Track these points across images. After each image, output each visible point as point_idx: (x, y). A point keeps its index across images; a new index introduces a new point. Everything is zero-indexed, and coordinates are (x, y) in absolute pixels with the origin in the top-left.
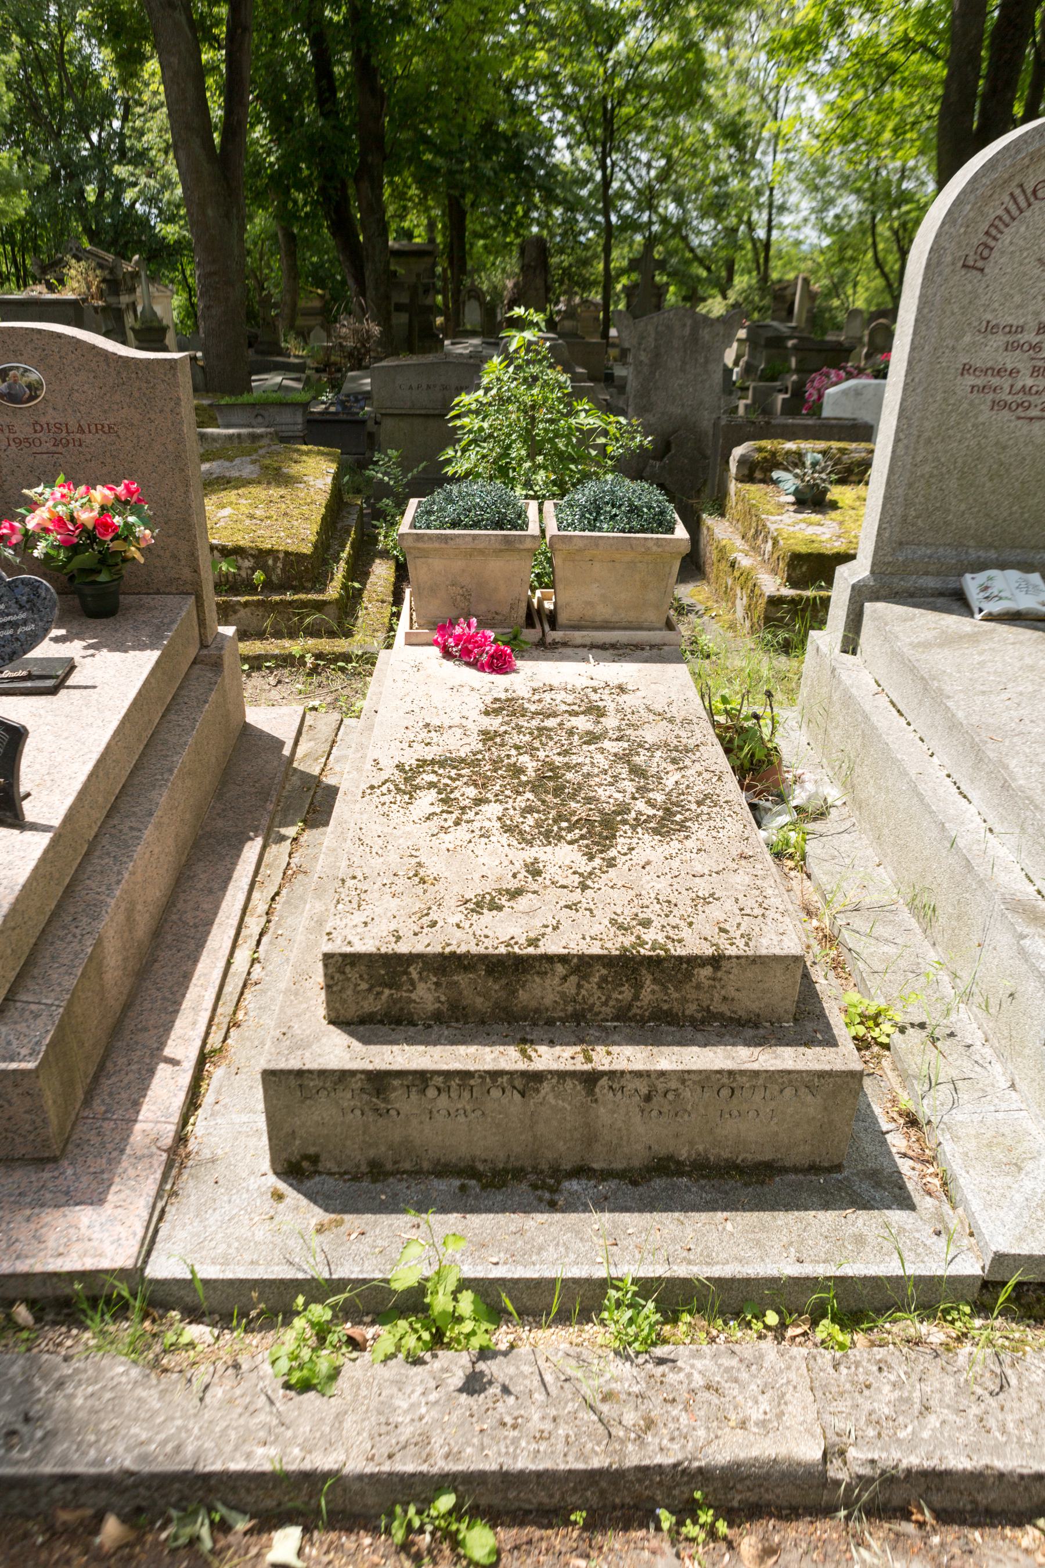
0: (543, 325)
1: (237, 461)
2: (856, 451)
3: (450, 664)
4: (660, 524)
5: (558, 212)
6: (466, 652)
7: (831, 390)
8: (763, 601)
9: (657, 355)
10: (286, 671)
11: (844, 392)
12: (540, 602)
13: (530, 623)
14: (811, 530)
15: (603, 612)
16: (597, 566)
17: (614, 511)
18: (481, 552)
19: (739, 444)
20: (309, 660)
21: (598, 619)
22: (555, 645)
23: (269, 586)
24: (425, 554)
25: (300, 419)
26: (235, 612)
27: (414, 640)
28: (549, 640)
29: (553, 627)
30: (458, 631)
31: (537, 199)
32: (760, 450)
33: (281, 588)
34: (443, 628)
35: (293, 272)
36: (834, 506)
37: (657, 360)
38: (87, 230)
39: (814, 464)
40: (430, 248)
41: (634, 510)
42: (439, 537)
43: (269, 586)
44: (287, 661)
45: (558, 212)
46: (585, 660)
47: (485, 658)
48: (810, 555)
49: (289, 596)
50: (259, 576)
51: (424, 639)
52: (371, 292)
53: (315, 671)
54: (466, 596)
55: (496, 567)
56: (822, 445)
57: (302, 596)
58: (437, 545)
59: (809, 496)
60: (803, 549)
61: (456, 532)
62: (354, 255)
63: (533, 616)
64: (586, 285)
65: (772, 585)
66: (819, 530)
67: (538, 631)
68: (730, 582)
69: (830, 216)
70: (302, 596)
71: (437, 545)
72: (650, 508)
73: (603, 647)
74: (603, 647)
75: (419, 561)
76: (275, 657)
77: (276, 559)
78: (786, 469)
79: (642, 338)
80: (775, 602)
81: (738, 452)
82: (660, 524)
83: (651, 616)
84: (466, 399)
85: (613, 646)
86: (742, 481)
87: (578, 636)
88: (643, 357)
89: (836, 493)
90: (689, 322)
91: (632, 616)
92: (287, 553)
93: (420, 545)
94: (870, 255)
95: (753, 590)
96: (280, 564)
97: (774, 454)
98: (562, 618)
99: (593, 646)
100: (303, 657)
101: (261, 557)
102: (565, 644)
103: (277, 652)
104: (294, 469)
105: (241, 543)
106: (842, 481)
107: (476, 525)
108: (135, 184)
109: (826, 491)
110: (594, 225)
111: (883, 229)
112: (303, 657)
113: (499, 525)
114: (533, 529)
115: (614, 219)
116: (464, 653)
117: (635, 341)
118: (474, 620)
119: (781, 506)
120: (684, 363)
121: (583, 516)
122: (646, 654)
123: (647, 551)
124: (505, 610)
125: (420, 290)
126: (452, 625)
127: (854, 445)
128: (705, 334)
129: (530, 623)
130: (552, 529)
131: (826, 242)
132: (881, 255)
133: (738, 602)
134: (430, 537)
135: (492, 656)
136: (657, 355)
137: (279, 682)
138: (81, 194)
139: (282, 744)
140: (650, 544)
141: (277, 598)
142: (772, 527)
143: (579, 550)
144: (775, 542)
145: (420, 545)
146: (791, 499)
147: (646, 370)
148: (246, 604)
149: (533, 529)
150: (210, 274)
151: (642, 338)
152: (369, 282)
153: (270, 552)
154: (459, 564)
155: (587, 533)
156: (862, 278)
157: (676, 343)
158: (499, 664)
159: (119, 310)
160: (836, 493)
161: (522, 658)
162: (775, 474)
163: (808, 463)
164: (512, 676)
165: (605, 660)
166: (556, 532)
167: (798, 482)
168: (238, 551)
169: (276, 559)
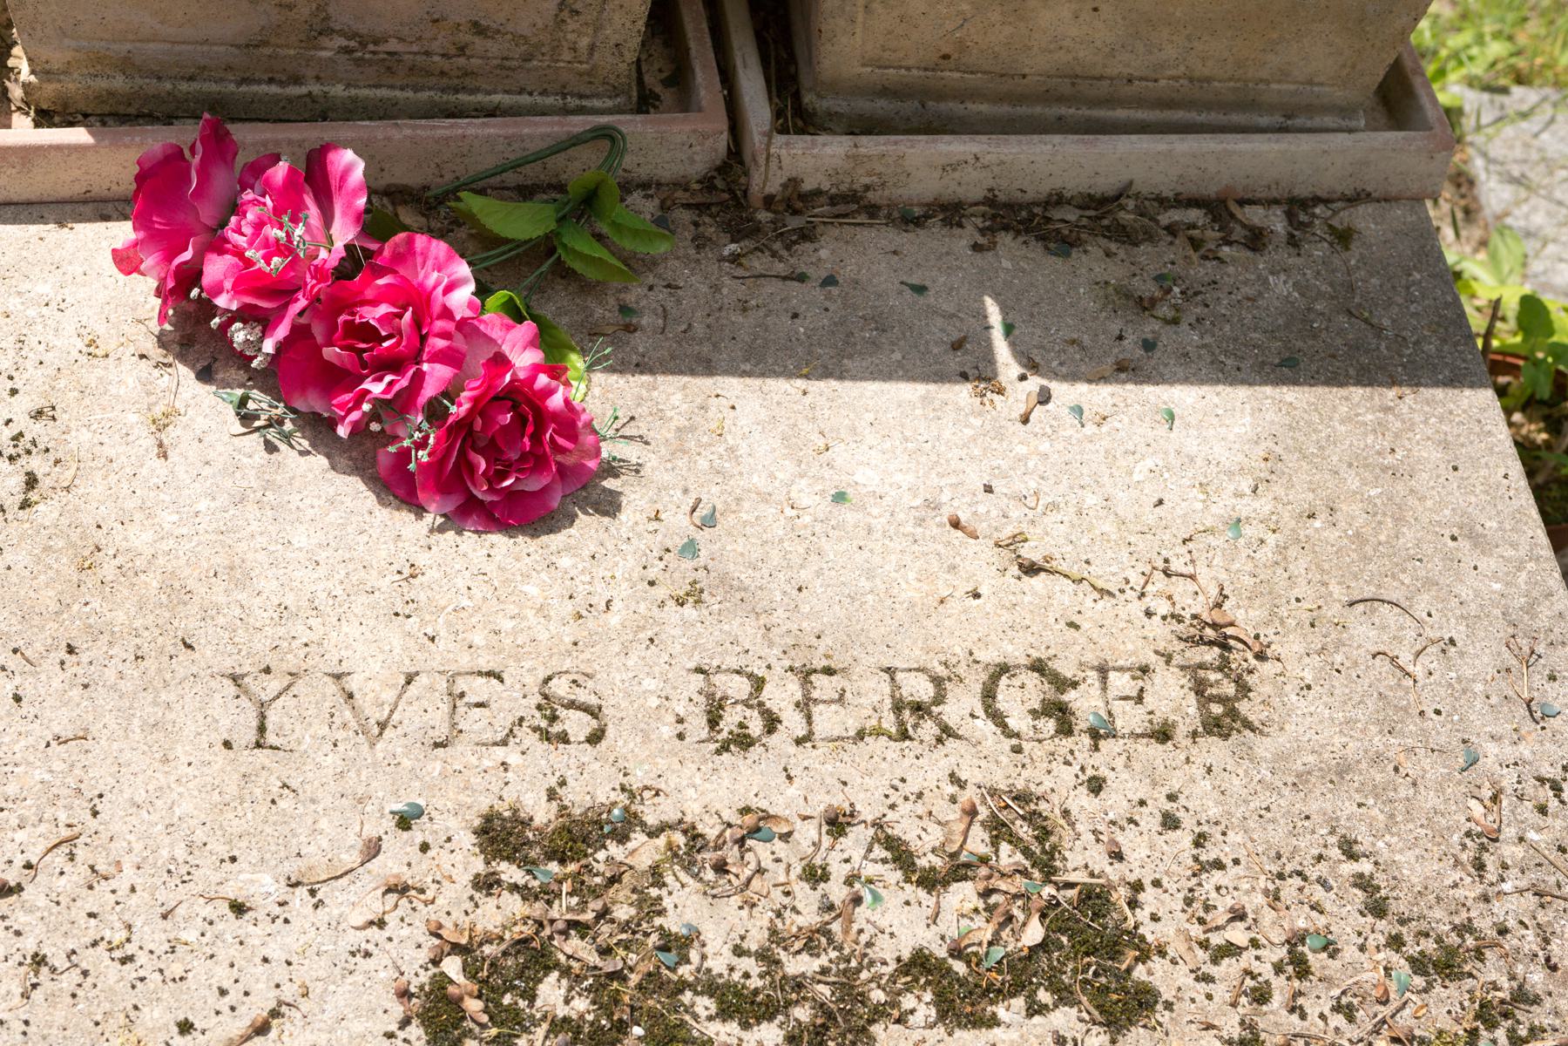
21: (1037, 63)
28: (765, 180)
83: (1319, 59)
85: (1104, 217)
87: (922, 164)
122: (1277, 282)
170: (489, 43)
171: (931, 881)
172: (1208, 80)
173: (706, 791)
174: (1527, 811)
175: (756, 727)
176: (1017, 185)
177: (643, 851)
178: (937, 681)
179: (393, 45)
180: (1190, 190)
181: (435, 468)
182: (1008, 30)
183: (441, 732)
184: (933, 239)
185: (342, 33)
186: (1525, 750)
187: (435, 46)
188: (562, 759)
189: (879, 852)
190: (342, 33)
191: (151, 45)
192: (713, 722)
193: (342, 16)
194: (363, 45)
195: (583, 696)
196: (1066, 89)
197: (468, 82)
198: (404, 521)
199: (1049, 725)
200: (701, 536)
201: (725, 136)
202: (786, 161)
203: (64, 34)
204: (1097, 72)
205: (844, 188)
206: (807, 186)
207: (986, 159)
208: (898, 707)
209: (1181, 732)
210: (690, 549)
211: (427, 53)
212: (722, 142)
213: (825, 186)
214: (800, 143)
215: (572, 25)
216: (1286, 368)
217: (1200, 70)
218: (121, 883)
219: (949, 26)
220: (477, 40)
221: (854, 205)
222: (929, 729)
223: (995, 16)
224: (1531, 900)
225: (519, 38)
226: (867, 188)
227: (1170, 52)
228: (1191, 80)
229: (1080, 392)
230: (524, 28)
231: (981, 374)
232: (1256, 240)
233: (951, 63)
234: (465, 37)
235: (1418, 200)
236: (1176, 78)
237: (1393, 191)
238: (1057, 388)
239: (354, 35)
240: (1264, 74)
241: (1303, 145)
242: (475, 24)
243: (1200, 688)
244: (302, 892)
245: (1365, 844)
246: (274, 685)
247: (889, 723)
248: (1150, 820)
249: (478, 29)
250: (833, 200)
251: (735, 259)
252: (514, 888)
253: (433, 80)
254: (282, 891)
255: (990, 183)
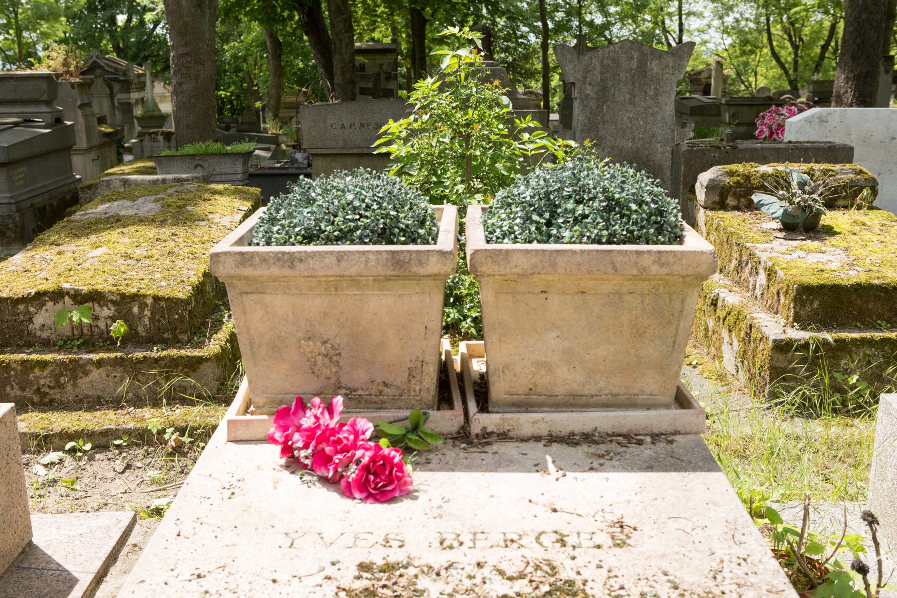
0: (479, 43)
1: (141, 200)
2: (842, 172)
3: (295, 479)
4: (660, 231)
5: (501, 22)
6: (322, 460)
7: (794, 119)
8: (765, 349)
9: (604, 88)
10: (140, 452)
11: (808, 120)
12: (465, 361)
13: (444, 399)
14: (813, 258)
15: (567, 379)
16: (555, 301)
17: (580, 209)
18: (354, 281)
19: (705, 169)
20: (171, 437)
21: (560, 390)
22: (486, 438)
23: (131, 339)
24: (257, 287)
25: (239, 169)
26: (86, 373)
27: (242, 434)
28: (475, 429)
29: (484, 406)
30: (307, 421)
31: (484, 11)
32: (731, 174)
33: (149, 342)
34: (284, 416)
35: (279, 71)
36: (830, 231)
37: (604, 93)
38: (117, 49)
39: (802, 185)
40: (393, 47)
41: (613, 206)
42: (279, 258)
43: (131, 339)
44: (143, 438)
45: (501, 22)
46: (539, 467)
47: (353, 473)
48: (822, 287)
49: (156, 353)
50: (119, 328)
51: (261, 433)
52: (338, 79)
53: (179, 450)
54: (333, 356)
55: (381, 307)
56: (805, 167)
57: (173, 352)
58: (275, 271)
59: (800, 220)
60: (812, 280)
61: (311, 248)
62: (324, 48)
63: (451, 385)
64: (530, 74)
65: (775, 327)
66: (824, 258)
67: (459, 411)
68: (711, 323)
69: (729, 20)
70: (173, 352)
71: (275, 271)
72: (640, 203)
73: (570, 440)
74: (570, 440)
75: (249, 300)
76: (129, 432)
77: (143, 306)
78: (772, 193)
79: (587, 71)
80: (782, 347)
81: (704, 178)
82: (660, 231)
83: (650, 384)
84: (393, 126)
85: (588, 438)
86: (712, 209)
87: (527, 422)
88: (589, 91)
89: (829, 218)
90: (636, 55)
91: (616, 385)
92: (156, 299)
93: (247, 271)
94: (766, 50)
95: (750, 336)
96: (147, 313)
97: (747, 177)
98: (498, 390)
99: (553, 439)
100: (161, 432)
101: (124, 303)
102: (504, 436)
103: (131, 425)
104: (201, 208)
105: (99, 287)
106: (830, 205)
107: (345, 236)
108: (153, 10)
109: (818, 214)
110: (534, 30)
111: (776, 30)
112: (161, 432)
113: (385, 236)
114: (446, 241)
115: (551, 25)
116: (318, 457)
117: (580, 76)
118: (339, 400)
119: (767, 232)
120: (633, 96)
121: (527, 218)
122: (647, 451)
123: (642, 275)
124: (400, 379)
125: (383, 77)
126: (302, 406)
127: (838, 167)
128: (654, 66)
129: (444, 399)
130: (476, 239)
131: (729, 41)
132: (777, 49)
133: (725, 347)
134: (264, 259)
135: (366, 469)
136: (604, 88)
137: (128, 467)
138: (113, 21)
139: (72, 582)
140: (647, 261)
141: (139, 355)
142: (764, 257)
143: (523, 275)
144: (771, 273)
145: (247, 271)
146: (776, 225)
147: (592, 104)
148: (100, 363)
149: (446, 241)
150: (184, 55)
151: (587, 71)
152: (337, 70)
153: (136, 297)
154: (316, 303)
155: (535, 246)
156: (761, 70)
157: (623, 76)
158: (380, 483)
159: (129, 104)
160: (829, 218)
161: (424, 465)
162: (756, 198)
163: (794, 184)
164: (403, 507)
165: (576, 467)
166: (483, 245)
167: (786, 204)
168: (95, 297)
169: (143, 306)
170: (389, 390)
171: (511, 579)
172: (617, 395)
173: (439, 559)
174: (734, 565)
175: (456, 544)
176: (558, 429)
177: (412, 571)
178: (520, 536)
179: (360, 392)
180: (617, 431)
181: (357, 481)
182: (548, 377)
183: (351, 544)
184: (531, 444)
185: (344, 388)
186: (733, 551)
187: (373, 392)
188: (387, 551)
189: (494, 572)
190: (344, 388)
191: (289, 396)
192: (441, 543)
193: (344, 382)
194: (351, 392)
195: (398, 538)
196: (571, 400)
197: (383, 405)
198: (349, 502)
199: (559, 545)
200: (443, 505)
201: (462, 416)
202: (481, 421)
203: (263, 392)
204: (580, 393)
205: (501, 431)
206: (489, 430)
207: (546, 419)
208: (505, 541)
209: (605, 547)
210: (440, 507)
211: (370, 395)
212: (462, 419)
213: (495, 430)
214: (485, 415)
215: (413, 382)
216: (650, 468)
217: (615, 391)
218: (238, 576)
219: (530, 377)
220: (385, 388)
221: (504, 436)
222: (515, 545)
223: (543, 372)
224: (735, 587)
225: (398, 387)
226: (509, 431)
227: (602, 384)
228: (612, 395)
229: (578, 474)
230: (399, 384)
231: (545, 470)
232: (640, 443)
233: (533, 392)
234: (381, 388)
235: (697, 433)
236: (606, 395)
237: (688, 430)
238: (567, 473)
239: (348, 389)
240: (635, 391)
241: (652, 413)
242: (384, 382)
243: (613, 538)
244: (297, 579)
245: (671, 571)
246: (297, 535)
247: (503, 544)
248: (592, 566)
249: (386, 385)
250: (498, 435)
251: (464, 449)
252: (367, 578)
253: (373, 405)
254: (290, 578)
255: (549, 429)
